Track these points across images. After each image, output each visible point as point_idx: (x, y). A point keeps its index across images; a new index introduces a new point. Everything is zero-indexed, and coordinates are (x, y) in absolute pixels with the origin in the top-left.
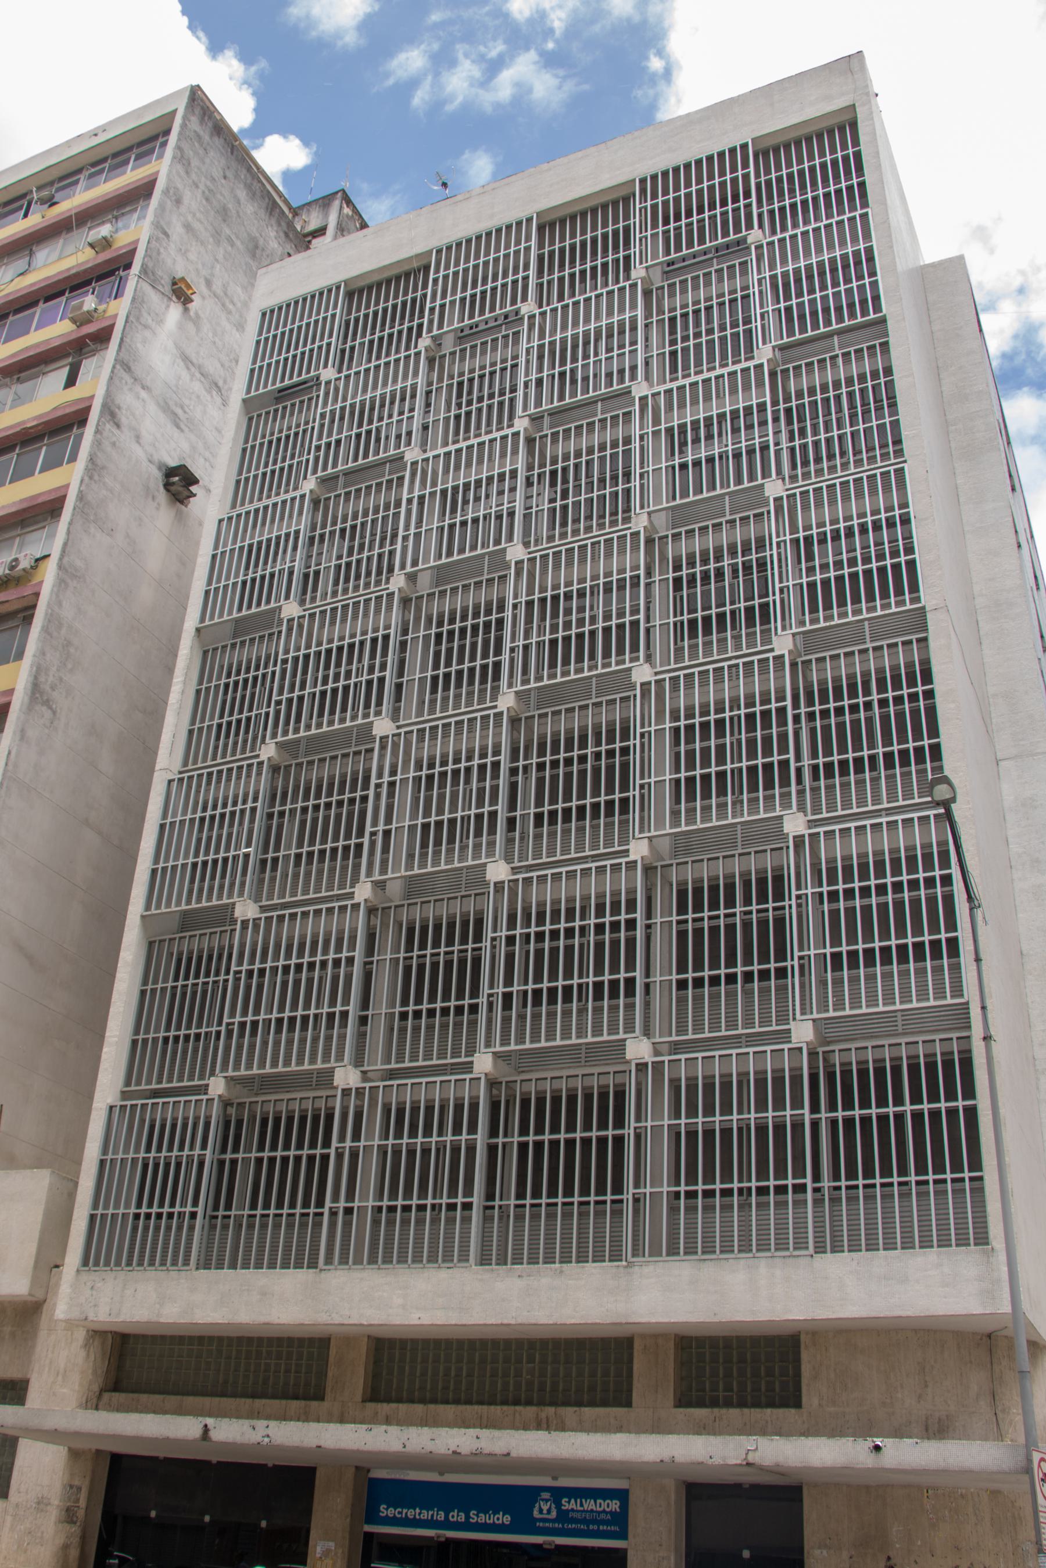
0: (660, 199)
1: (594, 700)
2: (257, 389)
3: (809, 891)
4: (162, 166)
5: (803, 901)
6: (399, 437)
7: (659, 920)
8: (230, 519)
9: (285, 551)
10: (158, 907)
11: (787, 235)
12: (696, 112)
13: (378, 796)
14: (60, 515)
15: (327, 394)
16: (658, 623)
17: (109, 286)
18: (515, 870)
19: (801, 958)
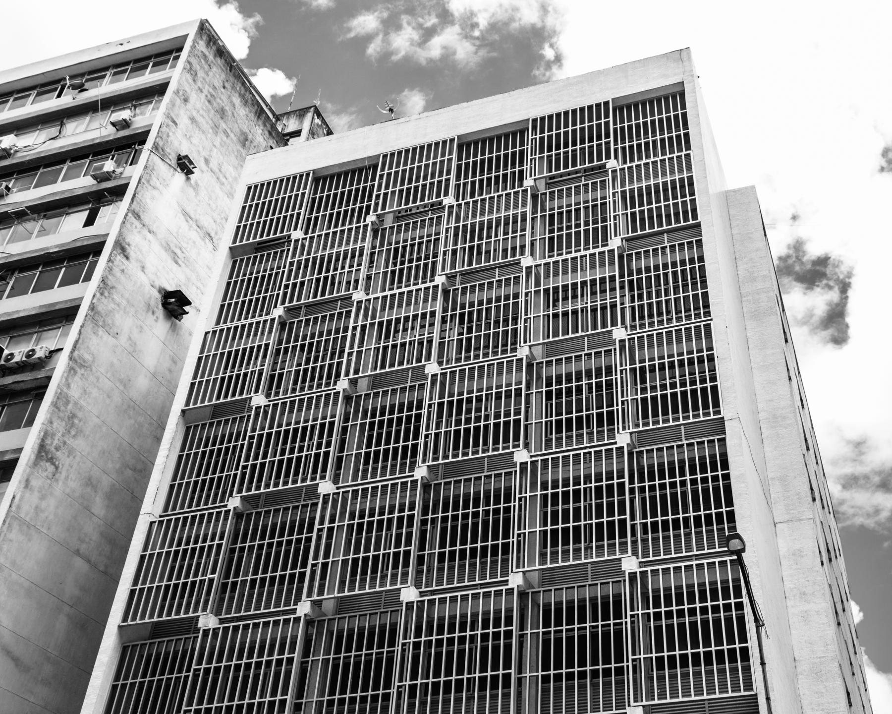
0: (546, 134)
1: (486, 474)
2: (241, 241)
3: (640, 612)
4: (175, 74)
5: (636, 619)
6: (348, 283)
7: (529, 631)
8: (214, 332)
9: (257, 358)
10: (134, 619)
11: (634, 164)
12: (574, 78)
13: (319, 538)
14: (74, 320)
15: (295, 249)
16: (534, 422)
17: (126, 156)
18: (422, 594)
19: (634, 660)
